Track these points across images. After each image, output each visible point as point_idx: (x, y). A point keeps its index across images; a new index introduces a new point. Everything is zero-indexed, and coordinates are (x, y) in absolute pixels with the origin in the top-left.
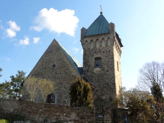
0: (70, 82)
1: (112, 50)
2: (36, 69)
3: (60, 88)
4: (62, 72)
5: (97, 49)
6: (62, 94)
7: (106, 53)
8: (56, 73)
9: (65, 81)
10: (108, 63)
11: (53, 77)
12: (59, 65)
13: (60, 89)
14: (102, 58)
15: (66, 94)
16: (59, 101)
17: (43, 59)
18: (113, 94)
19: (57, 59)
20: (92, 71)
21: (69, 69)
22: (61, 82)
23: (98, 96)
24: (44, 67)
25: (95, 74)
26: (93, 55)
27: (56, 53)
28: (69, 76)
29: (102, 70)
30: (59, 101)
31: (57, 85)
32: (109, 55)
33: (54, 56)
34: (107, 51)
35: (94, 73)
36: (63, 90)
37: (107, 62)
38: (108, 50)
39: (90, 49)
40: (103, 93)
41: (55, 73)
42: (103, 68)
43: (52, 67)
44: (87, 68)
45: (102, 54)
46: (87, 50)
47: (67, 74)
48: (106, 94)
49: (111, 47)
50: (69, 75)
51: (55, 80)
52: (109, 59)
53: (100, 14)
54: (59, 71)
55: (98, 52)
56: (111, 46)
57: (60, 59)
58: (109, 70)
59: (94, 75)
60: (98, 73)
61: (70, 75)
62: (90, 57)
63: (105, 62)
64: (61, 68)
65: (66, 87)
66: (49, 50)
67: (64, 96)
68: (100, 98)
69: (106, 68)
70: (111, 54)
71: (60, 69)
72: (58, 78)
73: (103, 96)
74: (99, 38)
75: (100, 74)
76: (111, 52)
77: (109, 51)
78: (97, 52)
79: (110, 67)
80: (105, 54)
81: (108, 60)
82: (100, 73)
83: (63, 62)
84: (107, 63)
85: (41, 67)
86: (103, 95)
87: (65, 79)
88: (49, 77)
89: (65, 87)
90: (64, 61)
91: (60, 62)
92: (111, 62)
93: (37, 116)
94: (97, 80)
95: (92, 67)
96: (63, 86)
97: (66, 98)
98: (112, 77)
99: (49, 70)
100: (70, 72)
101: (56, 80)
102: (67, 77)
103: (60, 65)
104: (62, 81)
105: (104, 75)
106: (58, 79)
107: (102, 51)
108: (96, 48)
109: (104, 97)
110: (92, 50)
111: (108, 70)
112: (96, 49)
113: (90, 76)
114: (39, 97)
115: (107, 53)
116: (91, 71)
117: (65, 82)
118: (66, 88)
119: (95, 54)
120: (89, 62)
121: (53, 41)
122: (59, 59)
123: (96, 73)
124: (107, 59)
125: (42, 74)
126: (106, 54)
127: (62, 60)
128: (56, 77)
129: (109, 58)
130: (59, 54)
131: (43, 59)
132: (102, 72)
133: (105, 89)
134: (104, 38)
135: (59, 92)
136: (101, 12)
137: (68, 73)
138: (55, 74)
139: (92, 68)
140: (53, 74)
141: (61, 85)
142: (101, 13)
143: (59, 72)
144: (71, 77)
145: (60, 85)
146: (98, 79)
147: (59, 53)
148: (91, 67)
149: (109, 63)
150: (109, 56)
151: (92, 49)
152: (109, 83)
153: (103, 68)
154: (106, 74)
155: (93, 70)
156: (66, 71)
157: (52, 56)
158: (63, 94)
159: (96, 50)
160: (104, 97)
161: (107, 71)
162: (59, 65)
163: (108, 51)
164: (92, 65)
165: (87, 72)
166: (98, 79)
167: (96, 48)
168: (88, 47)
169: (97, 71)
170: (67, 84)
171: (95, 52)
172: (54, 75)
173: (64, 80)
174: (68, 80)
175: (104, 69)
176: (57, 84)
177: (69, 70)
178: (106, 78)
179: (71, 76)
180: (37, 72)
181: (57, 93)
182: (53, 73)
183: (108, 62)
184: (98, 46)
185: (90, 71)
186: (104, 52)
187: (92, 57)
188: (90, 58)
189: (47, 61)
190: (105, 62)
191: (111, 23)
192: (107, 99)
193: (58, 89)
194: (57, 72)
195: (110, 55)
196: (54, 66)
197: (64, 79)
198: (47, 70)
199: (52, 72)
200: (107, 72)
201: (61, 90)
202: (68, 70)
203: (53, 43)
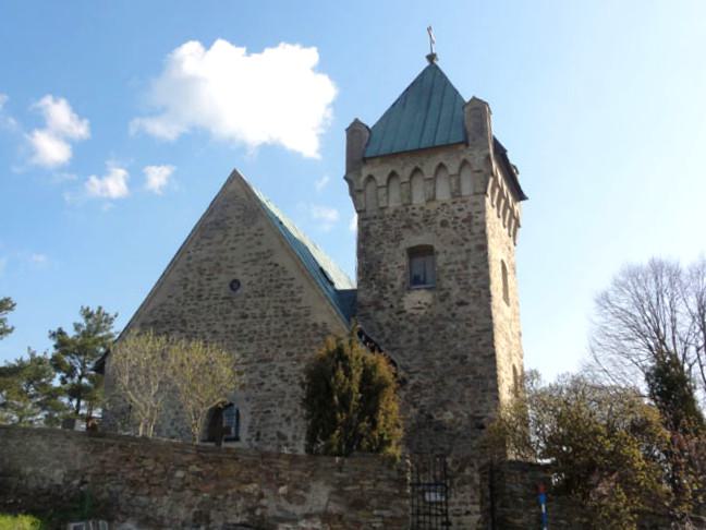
0: (302, 351)
1: (479, 212)
2: (157, 300)
3: (263, 380)
4: (270, 312)
5: (414, 211)
6: (272, 405)
7: (455, 228)
8: (245, 317)
9: (280, 350)
10: (465, 272)
11: (232, 332)
12: (254, 279)
13: (262, 384)
14: (436, 248)
15: (286, 405)
16: (258, 434)
17: (189, 258)
18: (485, 401)
19: (248, 258)
20: (396, 306)
21: (300, 295)
22: (267, 351)
23: (421, 412)
24: (192, 289)
25: (407, 318)
26: (398, 238)
27: (241, 231)
28: (298, 328)
29: (438, 301)
30: (258, 434)
31: (248, 367)
32: (468, 237)
33: (231, 245)
34: (459, 221)
35: (405, 312)
36: (274, 385)
37: (460, 266)
38: (463, 215)
39: (386, 212)
40: (444, 397)
41: (238, 315)
42: (442, 289)
43: (225, 291)
44: (376, 292)
45: (436, 232)
46: (375, 217)
47: (288, 319)
48: (456, 400)
49: (475, 204)
50: (298, 325)
51: (239, 345)
52: (468, 251)
53: (427, 64)
54: (256, 305)
55: (422, 224)
56: (473, 199)
57: (257, 254)
58: (466, 300)
59: (402, 323)
60: (422, 312)
61: (301, 321)
62: (389, 247)
63: (450, 267)
64: (263, 296)
65: (286, 373)
66: (212, 219)
67: (279, 411)
68: (431, 417)
69: (456, 293)
70: (476, 230)
71: (259, 299)
72: (250, 336)
73: (446, 410)
74: (422, 164)
75: (431, 315)
76: (477, 224)
77: (468, 220)
78: (417, 224)
79: (474, 286)
80: (449, 231)
81: (464, 257)
82: (429, 311)
83: (271, 267)
84: (459, 270)
85: (180, 292)
86: (443, 405)
87: (283, 341)
88: (215, 332)
89: (282, 376)
90: (276, 265)
91: (258, 268)
92: (474, 267)
93: (166, 498)
94: (416, 342)
95: (396, 289)
96: (276, 370)
97: (288, 419)
98: (480, 328)
99: (212, 302)
100: (302, 312)
101: (244, 346)
102: (289, 333)
103: (260, 281)
104: (270, 348)
105: (447, 319)
106: (251, 340)
107: (439, 219)
108: (410, 207)
109: (448, 416)
110: (394, 216)
111: (463, 298)
112: (411, 211)
113: (388, 324)
114: (173, 416)
115: (459, 229)
116: (392, 306)
117: (284, 353)
118: (287, 381)
119: (407, 234)
120: (384, 265)
121: (230, 181)
122: (254, 257)
123: (412, 315)
124: (460, 253)
125: (184, 322)
126: (453, 233)
127: (269, 260)
128: (245, 332)
129: (466, 247)
130: (256, 235)
131: (189, 258)
132: (440, 309)
133: (451, 382)
134: (445, 162)
135: (259, 394)
136: (429, 53)
137: (295, 315)
138: (241, 321)
139: (395, 293)
140: (230, 322)
141: (267, 364)
142: (431, 57)
143: (257, 312)
144: (305, 333)
145: (262, 366)
146: (421, 339)
147: (254, 229)
148: (392, 286)
149: (466, 268)
150: (466, 240)
151: (396, 211)
152: (470, 355)
153: (442, 289)
154: (454, 315)
155: (400, 301)
156: (288, 307)
157: (225, 242)
158: (277, 403)
159: (414, 214)
160: (448, 416)
161: (461, 304)
162: (254, 279)
163: (464, 221)
164: (395, 279)
165: (373, 308)
166: (421, 339)
167: (410, 207)
168: (378, 204)
169: (418, 305)
170: (293, 360)
171: (408, 226)
172: (233, 326)
173: (279, 346)
174: (294, 345)
175: (447, 295)
176: (250, 362)
177: (299, 301)
178: (456, 336)
179: (307, 326)
180: (161, 310)
181: (247, 400)
182: (232, 314)
183: (465, 264)
184: (419, 199)
185: (386, 304)
186: (444, 224)
187: (397, 246)
188: (388, 250)
189: (205, 265)
190: (450, 267)
191: (474, 99)
192: (460, 424)
193: (255, 383)
194: (248, 309)
195: (472, 234)
196: (235, 285)
197: (276, 341)
198: (206, 304)
199: (228, 312)
200: (461, 309)
201: (266, 387)
202: (295, 303)
203: (231, 188)
